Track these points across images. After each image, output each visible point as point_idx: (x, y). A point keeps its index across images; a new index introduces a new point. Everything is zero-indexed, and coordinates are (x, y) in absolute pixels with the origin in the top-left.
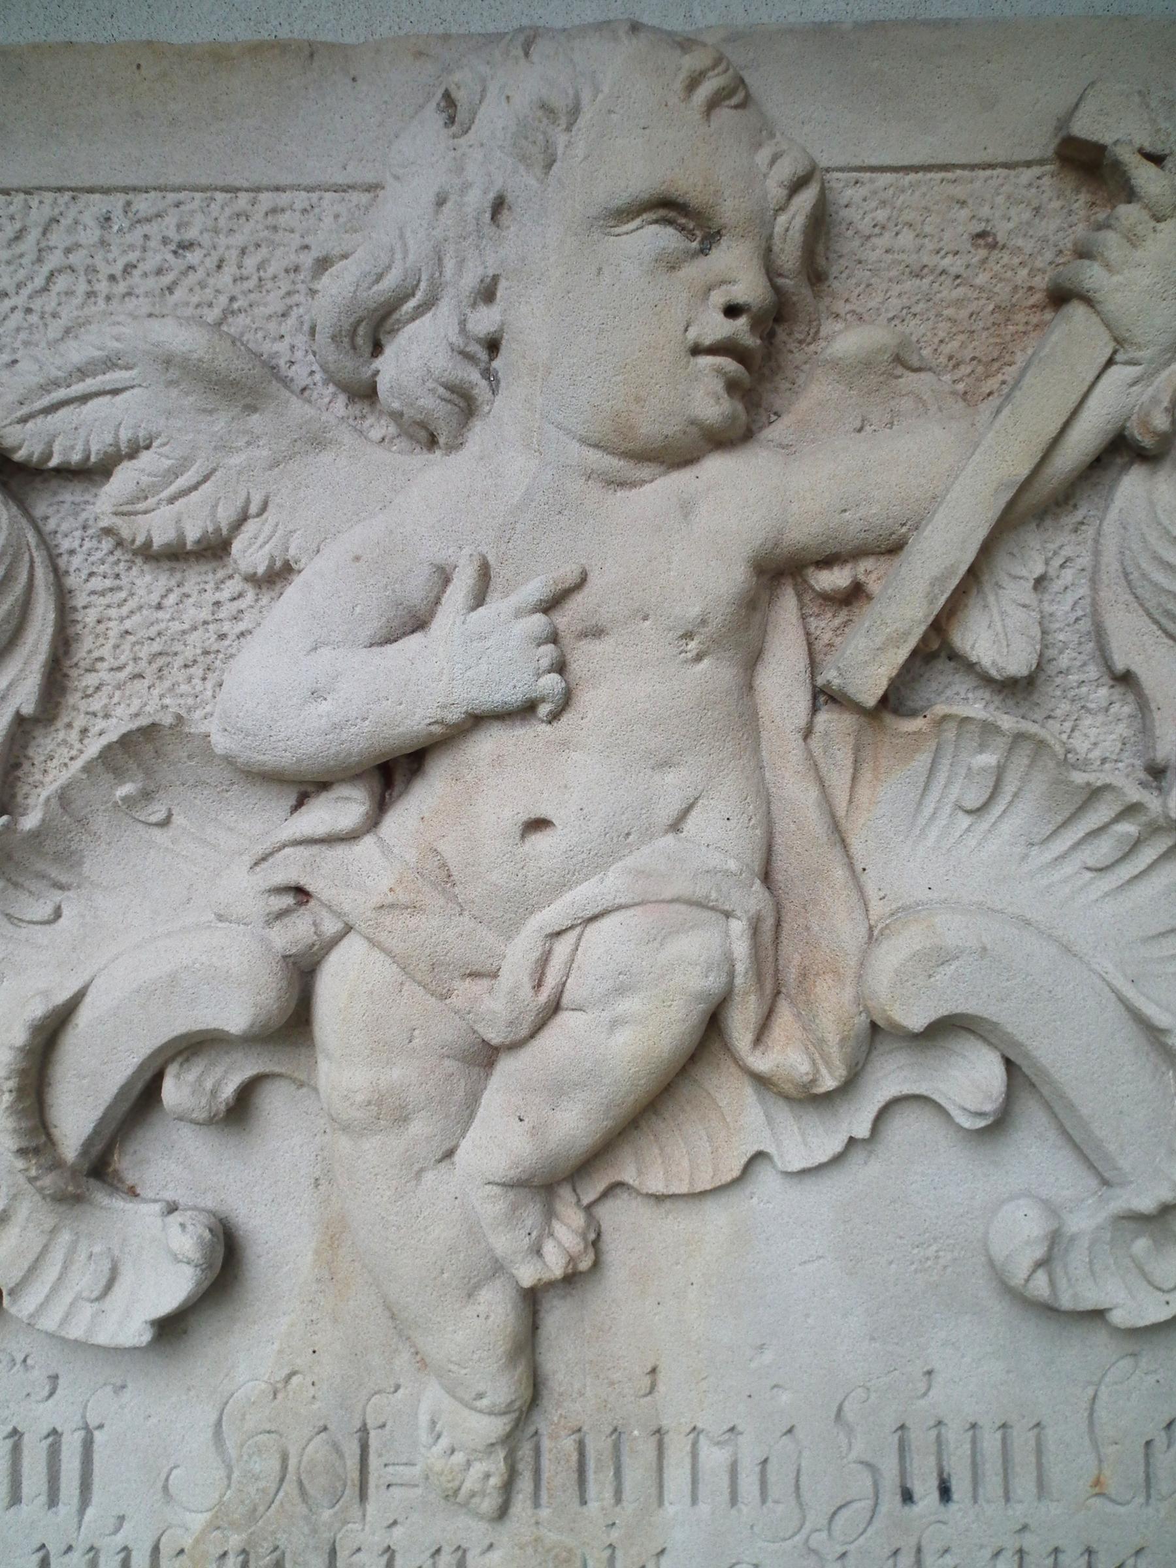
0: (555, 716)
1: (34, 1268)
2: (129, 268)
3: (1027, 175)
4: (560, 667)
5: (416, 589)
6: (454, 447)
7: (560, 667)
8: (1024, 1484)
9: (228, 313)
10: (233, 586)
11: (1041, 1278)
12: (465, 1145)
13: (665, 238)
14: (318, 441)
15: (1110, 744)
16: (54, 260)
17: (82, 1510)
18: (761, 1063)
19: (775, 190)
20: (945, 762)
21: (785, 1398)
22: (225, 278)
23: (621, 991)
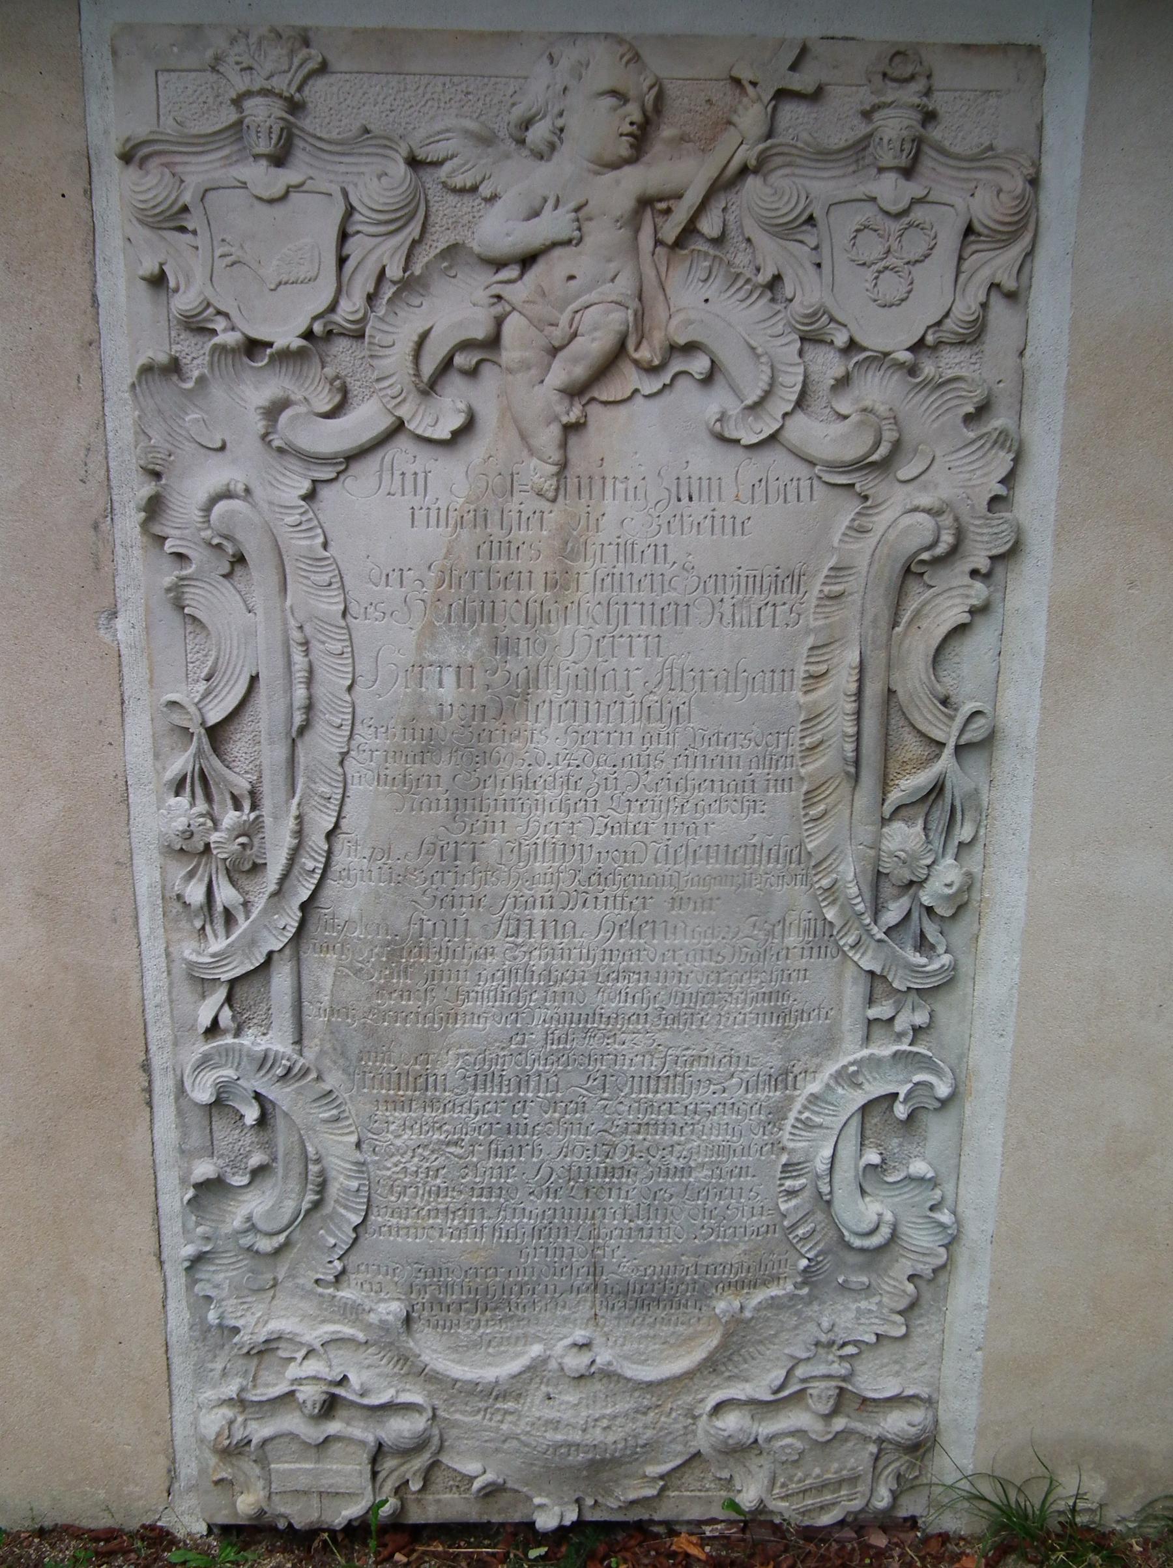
0: (577, 245)
1: (413, 416)
2: (451, 99)
3: (722, 83)
4: (579, 229)
5: (537, 203)
6: (549, 160)
7: (579, 229)
8: (715, 496)
9: (481, 114)
10: (478, 201)
11: (718, 424)
12: (547, 379)
13: (610, 101)
14: (508, 156)
15: (746, 261)
16: (428, 96)
17: (425, 496)
18: (636, 356)
19: (645, 89)
20: (694, 265)
21: (643, 468)
22: (480, 104)
23: (595, 329)
